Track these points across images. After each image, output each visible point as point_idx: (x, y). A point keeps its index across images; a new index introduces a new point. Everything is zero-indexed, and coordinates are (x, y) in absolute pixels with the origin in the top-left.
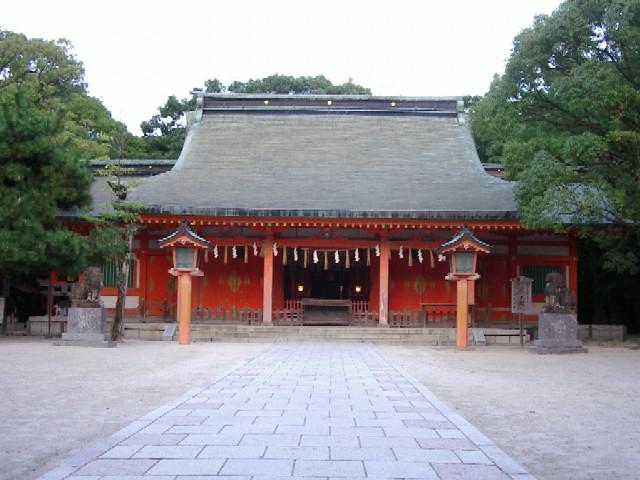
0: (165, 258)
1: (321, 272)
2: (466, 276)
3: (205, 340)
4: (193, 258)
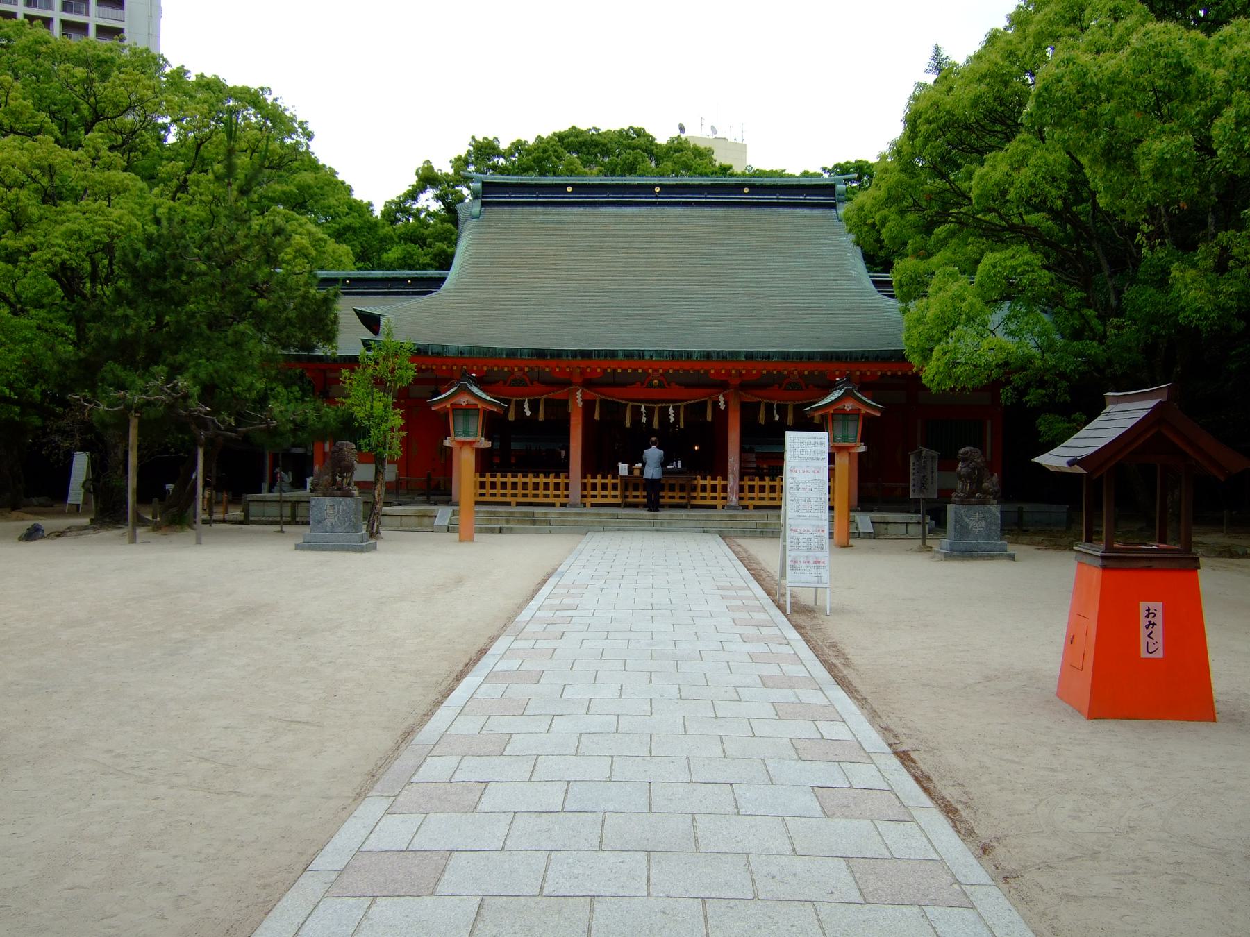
0: (441, 426)
1: (648, 436)
2: (847, 448)
3: (492, 531)
4: (476, 426)
